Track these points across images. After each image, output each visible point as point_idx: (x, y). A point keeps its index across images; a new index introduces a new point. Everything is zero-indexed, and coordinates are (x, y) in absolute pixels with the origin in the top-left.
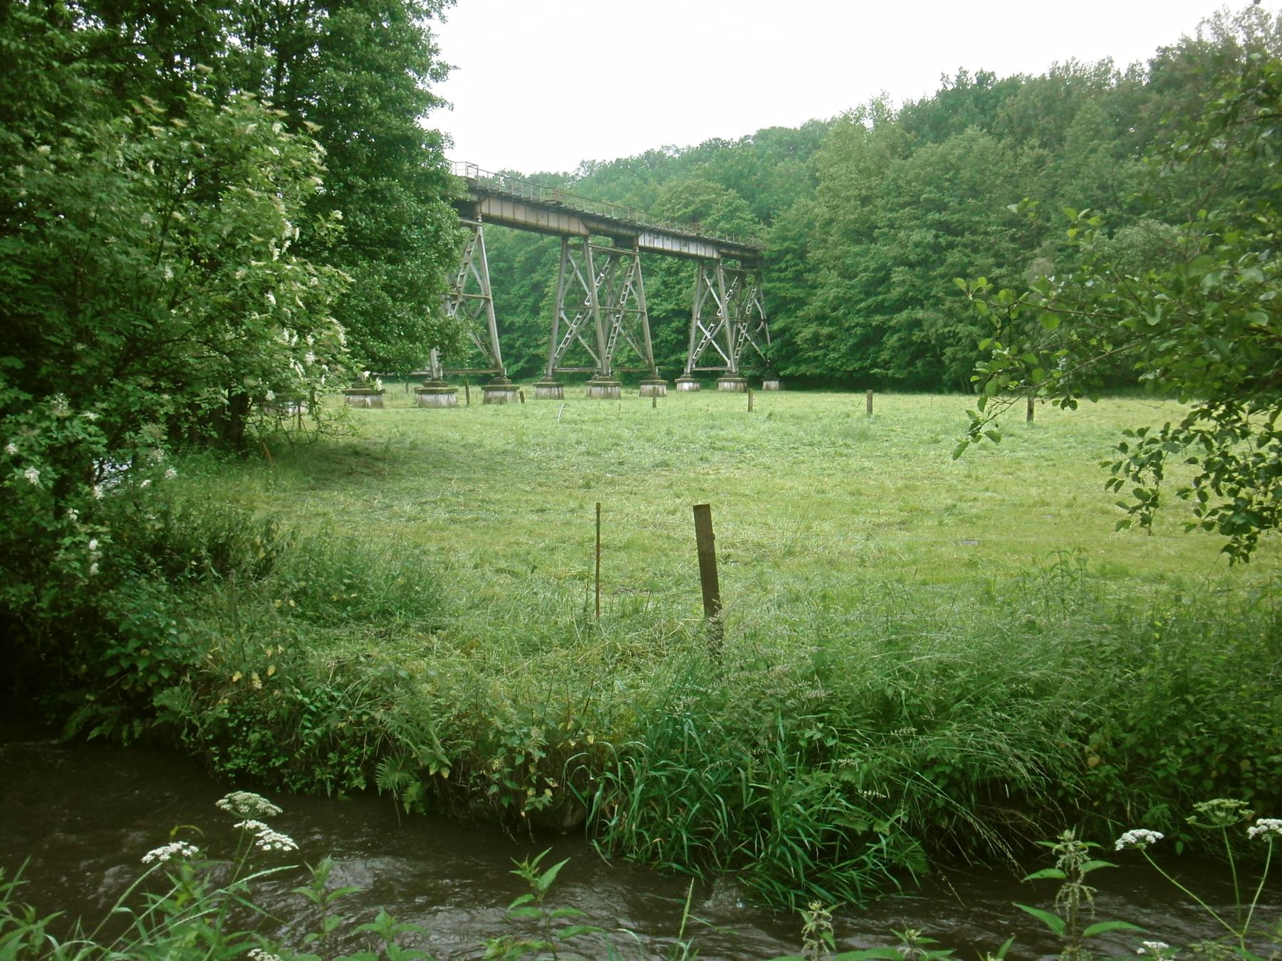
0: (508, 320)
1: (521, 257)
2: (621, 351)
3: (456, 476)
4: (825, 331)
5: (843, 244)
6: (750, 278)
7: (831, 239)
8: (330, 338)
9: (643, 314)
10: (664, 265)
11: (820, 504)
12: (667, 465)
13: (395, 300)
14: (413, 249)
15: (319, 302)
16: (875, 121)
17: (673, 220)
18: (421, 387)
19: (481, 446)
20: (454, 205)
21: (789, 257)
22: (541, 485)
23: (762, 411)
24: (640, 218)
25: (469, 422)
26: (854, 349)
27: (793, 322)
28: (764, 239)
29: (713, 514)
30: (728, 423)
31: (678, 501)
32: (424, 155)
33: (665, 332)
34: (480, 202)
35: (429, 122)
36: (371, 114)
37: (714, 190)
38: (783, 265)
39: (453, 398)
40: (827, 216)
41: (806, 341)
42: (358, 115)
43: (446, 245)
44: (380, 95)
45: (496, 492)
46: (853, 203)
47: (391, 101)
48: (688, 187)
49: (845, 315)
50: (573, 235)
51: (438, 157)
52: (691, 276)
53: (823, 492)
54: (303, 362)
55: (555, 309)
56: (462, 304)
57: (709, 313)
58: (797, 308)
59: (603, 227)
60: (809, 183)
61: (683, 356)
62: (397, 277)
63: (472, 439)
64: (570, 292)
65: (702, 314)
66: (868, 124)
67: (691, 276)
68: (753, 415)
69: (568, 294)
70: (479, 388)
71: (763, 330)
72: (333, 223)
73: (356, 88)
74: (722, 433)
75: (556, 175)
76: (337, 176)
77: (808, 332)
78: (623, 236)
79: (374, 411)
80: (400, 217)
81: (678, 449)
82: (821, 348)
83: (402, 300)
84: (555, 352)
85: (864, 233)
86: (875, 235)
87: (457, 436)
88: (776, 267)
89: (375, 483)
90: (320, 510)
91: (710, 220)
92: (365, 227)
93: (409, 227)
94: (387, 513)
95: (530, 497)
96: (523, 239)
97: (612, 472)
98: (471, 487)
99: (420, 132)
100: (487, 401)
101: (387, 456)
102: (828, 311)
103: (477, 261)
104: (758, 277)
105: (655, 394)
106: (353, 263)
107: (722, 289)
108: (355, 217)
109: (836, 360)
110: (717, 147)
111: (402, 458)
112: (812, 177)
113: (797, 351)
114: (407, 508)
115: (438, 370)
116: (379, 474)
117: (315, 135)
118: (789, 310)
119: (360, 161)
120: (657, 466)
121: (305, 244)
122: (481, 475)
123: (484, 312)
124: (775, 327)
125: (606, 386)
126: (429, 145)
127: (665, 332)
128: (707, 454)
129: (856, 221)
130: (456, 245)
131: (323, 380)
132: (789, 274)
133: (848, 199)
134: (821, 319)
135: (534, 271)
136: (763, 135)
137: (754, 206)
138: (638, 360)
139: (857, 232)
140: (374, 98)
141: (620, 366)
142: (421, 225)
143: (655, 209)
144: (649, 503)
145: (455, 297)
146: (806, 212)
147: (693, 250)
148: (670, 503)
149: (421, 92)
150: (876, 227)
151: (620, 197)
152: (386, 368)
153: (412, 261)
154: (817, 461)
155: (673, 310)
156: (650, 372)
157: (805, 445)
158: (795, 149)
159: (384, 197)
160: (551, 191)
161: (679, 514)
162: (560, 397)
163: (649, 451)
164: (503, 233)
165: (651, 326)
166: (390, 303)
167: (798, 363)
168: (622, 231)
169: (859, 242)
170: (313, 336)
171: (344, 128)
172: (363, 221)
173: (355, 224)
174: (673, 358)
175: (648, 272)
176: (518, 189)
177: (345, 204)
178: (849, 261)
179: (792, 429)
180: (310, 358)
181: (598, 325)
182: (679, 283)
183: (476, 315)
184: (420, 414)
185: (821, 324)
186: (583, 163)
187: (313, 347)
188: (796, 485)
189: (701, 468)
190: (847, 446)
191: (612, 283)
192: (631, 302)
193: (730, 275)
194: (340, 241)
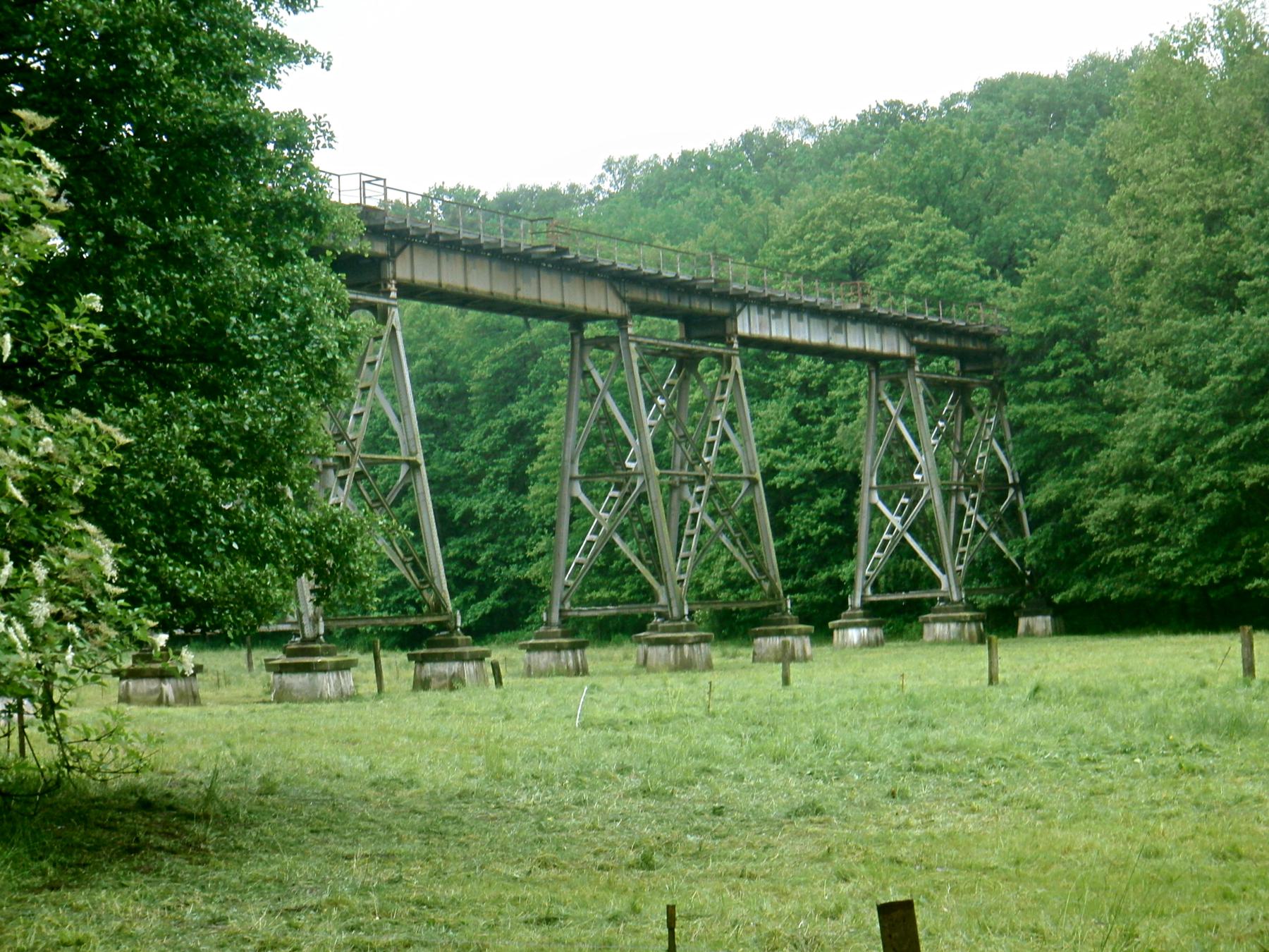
0: (460, 505)
1: (483, 370)
2: (708, 565)
3: (360, 851)
4: (1145, 502)
5: (1173, 315)
6: (980, 396)
7: (1146, 306)
8: (82, 567)
9: (753, 482)
10: (795, 376)
11: (1152, 881)
12: (819, 811)
13: (217, 474)
14: (252, 364)
15: (57, 488)
16: (1227, 51)
17: (809, 276)
18: (279, 657)
19: (411, 783)
20: (336, 266)
21: (1059, 348)
22: (545, 864)
23: (1018, 681)
24: (737, 274)
25: (384, 730)
26: (1207, 539)
27: (1076, 487)
28: (1005, 311)
29: (920, 914)
30: (947, 713)
31: (844, 888)
32: (271, 164)
33: (803, 520)
34: (392, 257)
35: (280, 95)
36: (159, 84)
37: (893, 211)
38: (1049, 365)
39: (348, 680)
40: (1136, 258)
41: (1106, 526)
42: (133, 89)
43: (323, 353)
44: (176, 43)
45: (448, 883)
46: (1188, 227)
47: (200, 54)
48: (837, 205)
49: (1185, 466)
50: (594, 318)
51: (301, 166)
52: (855, 396)
53: (1158, 854)
54: (25, 619)
55: (560, 480)
56: (359, 476)
57: (896, 476)
58: (1083, 457)
59: (659, 298)
60: (1095, 187)
61: (844, 572)
62: (219, 426)
63: (392, 770)
64: (594, 439)
65: (882, 478)
66: (1212, 58)
67: (855, 396)
68: (997, 692)
69: (587, 446)
70: (402, 657)
71: (1013, 507)
72: (81, 323)
73: (124, 32)
74: (934, 735)
75: (554, 192)
76: (91, 216)
77: (1109, 506)
78: (701, 315)
79: (179, 711)
80: (224, 299)
81: (841, 774)
82: (1138, 539)
83: (233, 474)
84: (563, 572)
85: (1217, 290)
86: (1239, 293)
87: (360, 765)
88: (1035, 370)
89: (187, 870)
90: (69, 934)
91: (888, 273)
92: (152, 323)
93: (244, 317)
94: (214, 934)
95: (523, 891)
96: (485, 330)
97: (698, 831)
98: (392, 873)
99: (263, 117)
100: (422, 684)
101: (213, 808)
102: (1148, 458)
103: (389, 381)
104: (997, 390)
105: (786, 657)
106: (128, 399)
107: (923, 420)
108: (129, 302)
109: (1171, 563)
110: (893, 120)
111: (243, 812)
112: (1100, 176)
113: (1087, 550)
114: (259, 923)
115: (315, 621)
116: (194, 851)
117: (40, 138)
118: (1066, 462)
119: (138, 183)
120: (797, 814)
121: (26, 361)
122: (414, 845)
123: (406, 491)
124: (1040, 499)
125: (678, 643)
126: (282, 144)
127: (803, 520)
128: (904, 782)
129: (1197, 264)
130: (344, 352)
131: (70, 656)
132: (1063, 384)
133: (1178, 220)
134: (1135, 477)
135: (512, 399)
136: (989, 91)
137: (980, 241)
138: (748, 583)
139: (1201, 288)
140: (165, 52)
141: (709, 598)
142: (268, 313)
143: (769, 254)
144: (783, 895)
145: (345, 462)
146: (1091, 251)
147: (855, 339)
148: (826, 895)
149: (264, 35)
150: (1242, 276)
151: (693, 232)
152: (200, 623)
153: (251, 389)
154: (1141, 788)
155: (819, 471)
156: (774, 609)
157: (1113, 752)
158: (1059, 119)
159: (190, 257)
160: (542, 226)
161: (846, 917)
162: (580, 670)
163: (777, 782)
164: (444, 319)
165: (773, 508)
166: (207, 482)
167: (1090, 575)
168: (700, 305)
169: (1205, 310)
170: (46, 563)
171: (102, 116)
172: (145, 308)
173: (131, 317)
174: (822, 576)
175: (761, 392)
176: (472, 226)
177: (110, 275)
178: (1186, 351)
179: (1085, 720)
180: (41, 609)
181: (656, 511)
182: (828, 411)
183: (391, 498)
184: (279, 715)
185: (1135, 489)
186: (609, 165)
187: (47, 585)
188: (1096, 841)
189: (893, 813)
190: (1202, 750)
191: (685, 419)
192: (727, 457)
193: (937, 389)
194: (99, 353)
